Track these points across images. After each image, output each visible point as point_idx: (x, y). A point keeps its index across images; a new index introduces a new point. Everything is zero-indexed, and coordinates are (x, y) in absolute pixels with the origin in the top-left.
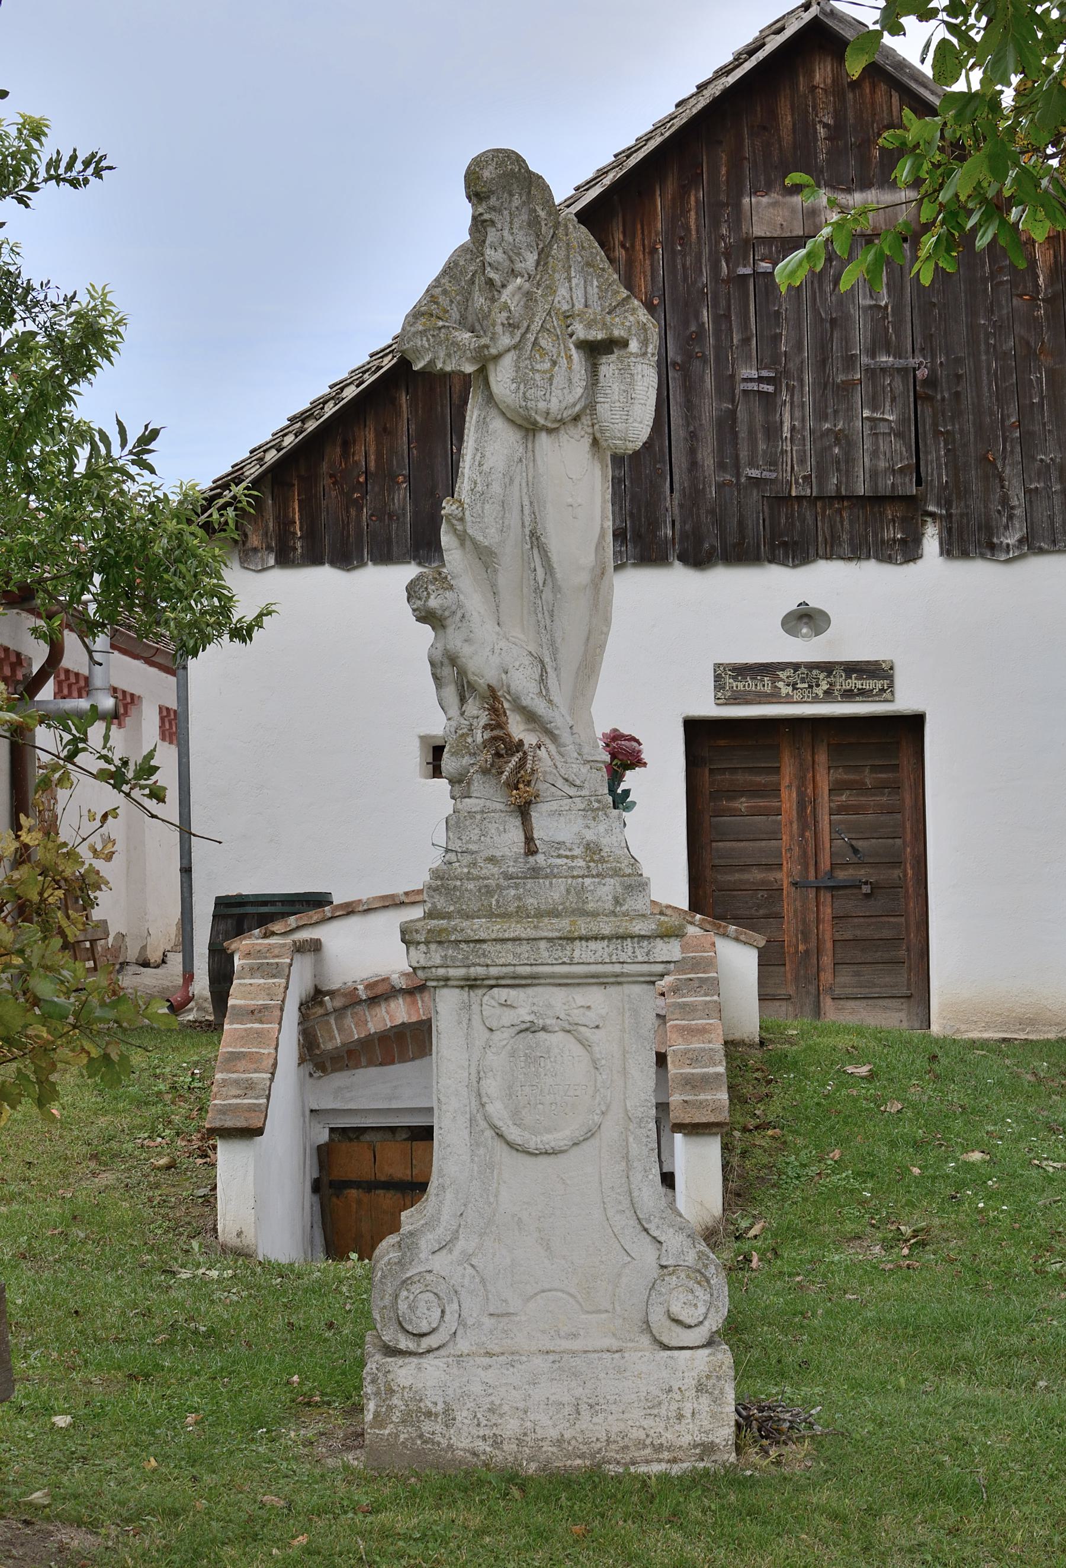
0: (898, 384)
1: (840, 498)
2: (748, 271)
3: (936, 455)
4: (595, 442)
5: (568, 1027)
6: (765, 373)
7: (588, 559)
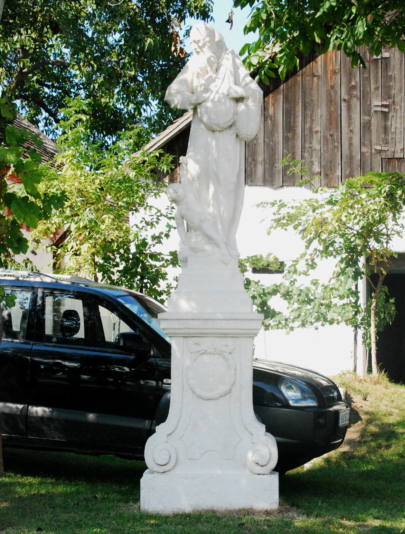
4: (237, 136)
5: (219, 353)
6: (385, 103)
7: (234, 179)
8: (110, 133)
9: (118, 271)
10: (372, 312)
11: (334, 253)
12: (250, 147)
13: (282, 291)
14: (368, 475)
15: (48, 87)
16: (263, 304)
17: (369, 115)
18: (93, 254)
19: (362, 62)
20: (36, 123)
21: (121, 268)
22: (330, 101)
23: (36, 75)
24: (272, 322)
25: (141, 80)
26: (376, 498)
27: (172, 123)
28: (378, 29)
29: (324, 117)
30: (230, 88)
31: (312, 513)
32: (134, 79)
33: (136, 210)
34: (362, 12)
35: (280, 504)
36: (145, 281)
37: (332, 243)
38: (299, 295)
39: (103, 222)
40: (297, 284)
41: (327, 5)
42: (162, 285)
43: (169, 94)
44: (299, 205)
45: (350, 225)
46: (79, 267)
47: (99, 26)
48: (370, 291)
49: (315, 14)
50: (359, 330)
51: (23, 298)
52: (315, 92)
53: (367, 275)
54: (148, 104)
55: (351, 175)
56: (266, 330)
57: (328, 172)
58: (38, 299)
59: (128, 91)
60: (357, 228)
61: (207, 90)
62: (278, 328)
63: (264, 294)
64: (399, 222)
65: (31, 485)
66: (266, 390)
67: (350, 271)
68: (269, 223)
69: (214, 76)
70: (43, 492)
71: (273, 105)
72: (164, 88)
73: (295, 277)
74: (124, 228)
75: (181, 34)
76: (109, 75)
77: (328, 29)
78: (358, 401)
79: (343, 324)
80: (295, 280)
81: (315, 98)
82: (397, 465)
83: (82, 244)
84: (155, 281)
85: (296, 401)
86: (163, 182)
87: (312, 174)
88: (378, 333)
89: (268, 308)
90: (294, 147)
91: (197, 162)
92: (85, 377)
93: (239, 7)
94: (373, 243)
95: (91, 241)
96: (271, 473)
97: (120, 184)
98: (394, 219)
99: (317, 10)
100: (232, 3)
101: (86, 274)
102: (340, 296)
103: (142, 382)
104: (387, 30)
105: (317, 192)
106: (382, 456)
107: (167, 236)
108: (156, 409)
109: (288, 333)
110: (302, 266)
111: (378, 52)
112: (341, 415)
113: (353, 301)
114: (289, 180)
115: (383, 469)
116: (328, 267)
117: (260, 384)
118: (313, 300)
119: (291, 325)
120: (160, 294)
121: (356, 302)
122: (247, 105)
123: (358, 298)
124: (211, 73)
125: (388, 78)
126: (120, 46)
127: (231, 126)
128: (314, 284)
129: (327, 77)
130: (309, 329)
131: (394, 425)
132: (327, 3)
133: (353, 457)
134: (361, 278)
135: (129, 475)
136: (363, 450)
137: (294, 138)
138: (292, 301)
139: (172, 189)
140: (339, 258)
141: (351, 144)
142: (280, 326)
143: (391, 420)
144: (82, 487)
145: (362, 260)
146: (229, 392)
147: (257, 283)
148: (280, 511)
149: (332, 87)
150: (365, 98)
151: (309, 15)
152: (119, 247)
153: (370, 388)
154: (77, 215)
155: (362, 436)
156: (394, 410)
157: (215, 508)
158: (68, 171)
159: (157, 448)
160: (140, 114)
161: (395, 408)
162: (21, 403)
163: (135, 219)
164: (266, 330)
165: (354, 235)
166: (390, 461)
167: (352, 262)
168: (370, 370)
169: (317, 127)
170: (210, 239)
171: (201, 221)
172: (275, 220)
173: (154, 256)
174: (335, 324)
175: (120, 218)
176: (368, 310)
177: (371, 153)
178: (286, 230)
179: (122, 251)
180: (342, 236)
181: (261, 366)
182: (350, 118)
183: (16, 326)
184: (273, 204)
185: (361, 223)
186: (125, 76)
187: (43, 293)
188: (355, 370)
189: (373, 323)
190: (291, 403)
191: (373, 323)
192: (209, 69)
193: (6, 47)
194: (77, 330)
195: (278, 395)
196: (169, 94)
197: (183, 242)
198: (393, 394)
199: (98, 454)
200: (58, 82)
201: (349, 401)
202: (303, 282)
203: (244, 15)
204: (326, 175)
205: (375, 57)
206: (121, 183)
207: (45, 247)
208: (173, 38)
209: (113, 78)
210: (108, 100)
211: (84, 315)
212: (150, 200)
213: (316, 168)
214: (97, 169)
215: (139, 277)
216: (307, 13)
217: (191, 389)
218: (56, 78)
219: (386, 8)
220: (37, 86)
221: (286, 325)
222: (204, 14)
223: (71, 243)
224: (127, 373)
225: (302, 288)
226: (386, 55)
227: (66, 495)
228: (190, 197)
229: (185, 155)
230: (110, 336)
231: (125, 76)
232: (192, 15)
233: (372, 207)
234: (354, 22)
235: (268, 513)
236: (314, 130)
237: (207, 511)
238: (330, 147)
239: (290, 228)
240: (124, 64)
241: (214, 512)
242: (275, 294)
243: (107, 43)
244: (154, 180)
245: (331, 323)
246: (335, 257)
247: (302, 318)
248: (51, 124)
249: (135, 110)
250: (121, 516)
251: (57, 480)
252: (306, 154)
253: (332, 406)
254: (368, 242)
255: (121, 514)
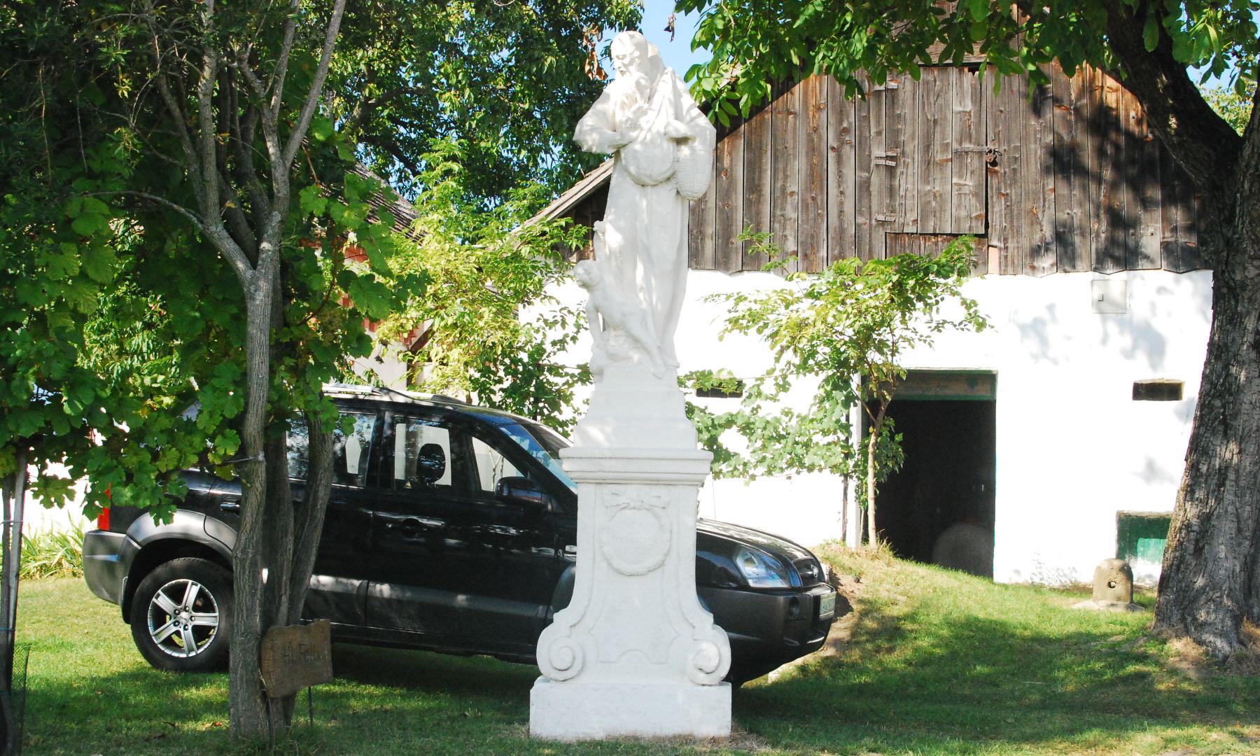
0: (976, 163)
1: (935, 235)
2: (882, 88)
3: (998, 207)
4: (678, 192)
6: (890, 154)
8: (491, 194)
9: (501, 389)
10: (870, 457)
11: (816, 368)
12: (697, 212)
13: (740, 422)
14: (861, 690)
15: (404, 125)
16: (712, 443)
17: (868, 170)
18: (466, 364)
19: (861, 92)
20: (386, 176)
21: (506, 384)
22: (812, 149)
23: (387, 107)
24: (724, 467)
25: (538, 116)
26: (873, 722)
27: (582, 178)
28: (882, 47)
29: (803, 173)
30: (668, 124)
31: (779, 743)
32: (528, 115)
33: (529, 303)
34: (861, 20)
35: (734, 729)
36: (541, 405)
37: (813, 354)
38: (765, 428)
39: (481, 317)
40: (761, 413)
41: (810, 10)
42: (565, 413)
43: (581, 131)
44: (765, 298)
45: (839, 329)
46: (447, 378)
47: (479, 39)
48: (867, 423)
49: (794, 22)
50: (850, 481)
51: (365, 427)
52: (789, 136)
53: (863, 401)
54: (548, 151)
55: (841, 256)
56: (715, 478)
57: (809, 252)
58: (386, 427)
59: (519, 132)
60: (850, 332)
61: (635, 126)
62: (733, 476)
63: (714, 426)
64: (911, 324)
65: (371, 697)
66: (715, 562)
67: (840, 396)
68: (721, 325)
69: (646, 106)
70: (389, 706)
71: (730, 154)
72: (571, 129)
73: (759, 402)
74: (511, 326)
75: (599, 49)
76: (492, 108)
77: (812, 45)
78: (847, 583)
79: (827, 471)
80: (759, 407)
81: (790, 144)
82: (903, 676)
83: (450, 349)
84: (555, 406)
85: (759, 579)
86: (569, 262)
87: (786, 254)
88: (878, 485)
89: (720, 447)
90: (758, 213)
91: (618, 229)
92: (452, 541)
93: (683, 12)
94: (873, 356)
95: (463, 345)
96: (720, 684)
97: (507, 264)
98: (903, 322)
99: (795, 18)
100: (674, 4)
101: (459, 393)
102: (823, 431)
103: (534, 550)
104: (896, 49)
105: (791, 279)
106: (881, 663)
107: (574, 339)
108: (552, 588)
109: (747, 484)
110: (769, 387)
111: (882, 79)
112: (823, 603)
113: (843, 437)
114: (752, 262)
115: (882, 682)
116: (806, 391)
117: (707, 556)
118: (783, 437)
119: (751, 472)
120: (563, 424)
121: (847, 439)
122: (692, 149)
123: (850, 434)
124: (641, 103)
125: (894, 118)
126: (510, 68)
127: (668, 179)
128: (787, 414)
129: (807, 114)
130: (778, 478)
131: (899, 619)
132: (811, 6)
133: (840, 665)
134: (855, 405)
135: (514, 688)
136: (855, 655)
137: (759, 202)
138: (753, 438)
139: (580, 269)
140: (823, 375)
141: (841, 212)
142: (736, 473)
143: (895, 611)
144: (442, 703)
145: (856, 379)
146: (662, 565)
147: (703, 411)
148: (733, 739)
149: (815, 130)
150: (862, 145)
151: (784, 25)
152: (504, 354)
153: (865, 564)
154: (443, 307)
155: (853, 635)
156: (900, 597)
157: (638, 734)
158: (431, 244)
159: (554, 645)
160: (536, 165)
161: (901, 594)
162: (358, 579)
163: (527, 315)
164: (715, 478)
165: (845, 343)
166: (893, 671)
167: (840, 383)
168: (865, 539)
169: (793, 187)
170: (636, 342)
171: (624, 315)
172: (730, 321)
173: (555, 370)
174: (816, 471)
175: (504, 311)
176: (864, 447)
177: (870, 225)
178: (746, 334)
179: (507, 361)
180: (829, 343)
181: (708, 528)
182: (840, 174)
183: (353, 466)
184: (728, 297)
185: (857, 326)
186: (516, 111)
187: (393, 418)
188: (844, 539)
189: (871, 471)
190: (752, 583)
191: (871, 471)
192: (638, 96)
193: (346, 68)
194: (440, 473)
195: (733, 571)
196: (581, 131)
197: (596, 346)
198: (898, 573)
199: (469, 654)
200: (420, 119)
201: (834, 582)
202: (769, 411)
203: (690, 23)
204: (806, 256)
205: (877, 88)
206: (506, 261)
207: (395, 354)
208: (586, 56)
209: (497, 112)
210: (489, 145)
211: (452, 451)
212: (550, 288)
213: (791, 246)
214: (473, 242)
215: (532, 399)
216: (781, 22)
217: (607, 560)
218: (416, 113)
219: (894, 17)
220: (389, 124)
221: (745, 471)
222: (631, 22)
223: (435, 349)
224: (512, 536)
225: (769, 418)
226: (893, 85)
227: (422, 713)
228: (609, 279)
229: (601, 219)
230: (488, 484)
231: (516, 111)
232: (612, 26)
233: (872, 303)
234: (848, 35)
235: (714, 741)
236: (789, 190)
237: (627, 738)
238: (811, 215)
239: (753, 331)
240: (514, 93)
241: (636, 739)
242: (730, 427)
243: (490, 63)
244: (556, 259)
245: (810, 469)
246: (817, 374)
247: (768, 461)
248: (407, 178)
249: (529, 159)
250: (501, 742)
251: (408, 689)
252: (777, 226)
253: (810, 589)
254: (865, 353)
255: (501, 740)
